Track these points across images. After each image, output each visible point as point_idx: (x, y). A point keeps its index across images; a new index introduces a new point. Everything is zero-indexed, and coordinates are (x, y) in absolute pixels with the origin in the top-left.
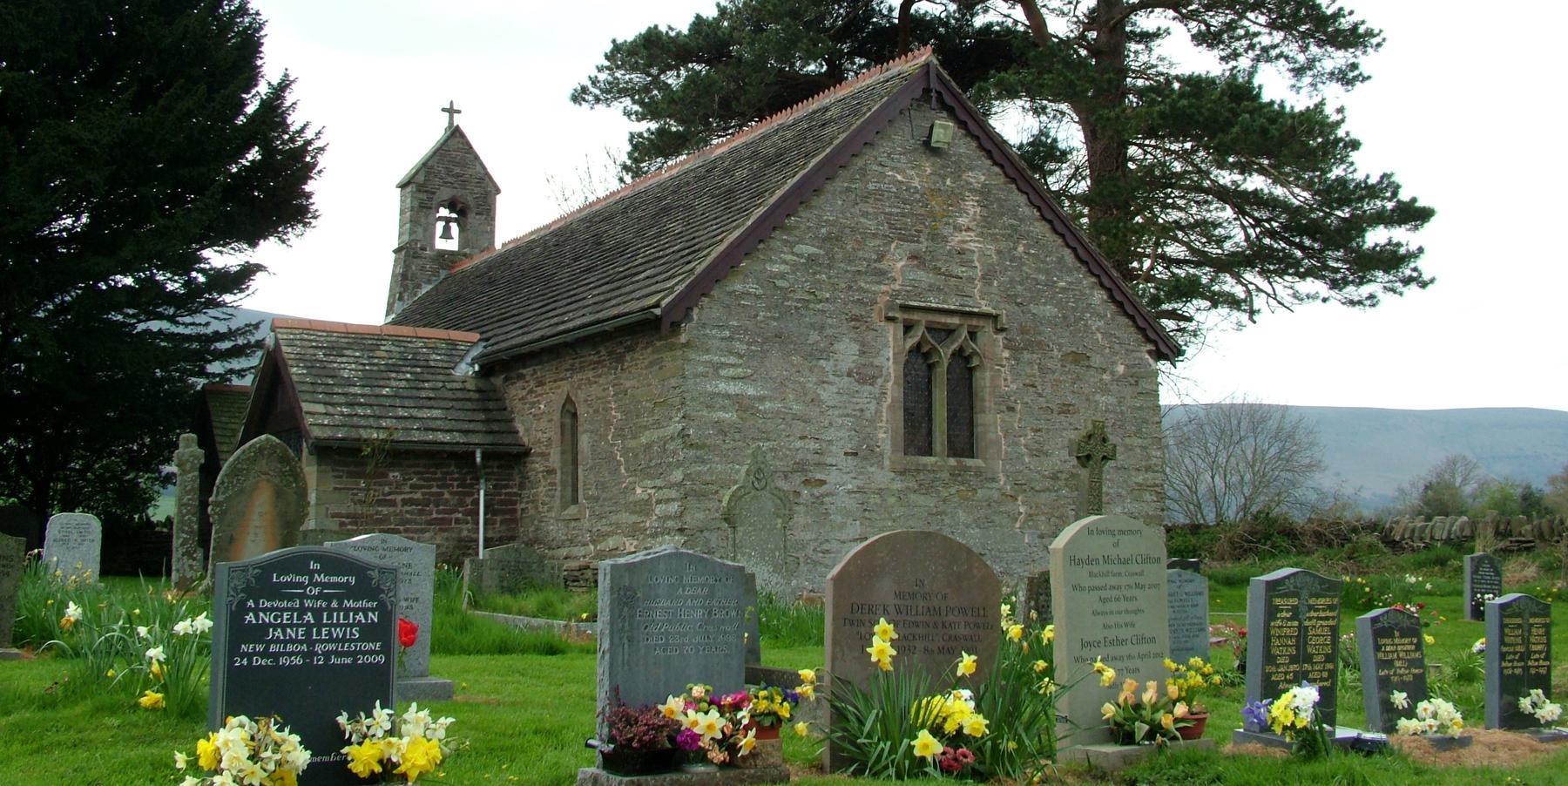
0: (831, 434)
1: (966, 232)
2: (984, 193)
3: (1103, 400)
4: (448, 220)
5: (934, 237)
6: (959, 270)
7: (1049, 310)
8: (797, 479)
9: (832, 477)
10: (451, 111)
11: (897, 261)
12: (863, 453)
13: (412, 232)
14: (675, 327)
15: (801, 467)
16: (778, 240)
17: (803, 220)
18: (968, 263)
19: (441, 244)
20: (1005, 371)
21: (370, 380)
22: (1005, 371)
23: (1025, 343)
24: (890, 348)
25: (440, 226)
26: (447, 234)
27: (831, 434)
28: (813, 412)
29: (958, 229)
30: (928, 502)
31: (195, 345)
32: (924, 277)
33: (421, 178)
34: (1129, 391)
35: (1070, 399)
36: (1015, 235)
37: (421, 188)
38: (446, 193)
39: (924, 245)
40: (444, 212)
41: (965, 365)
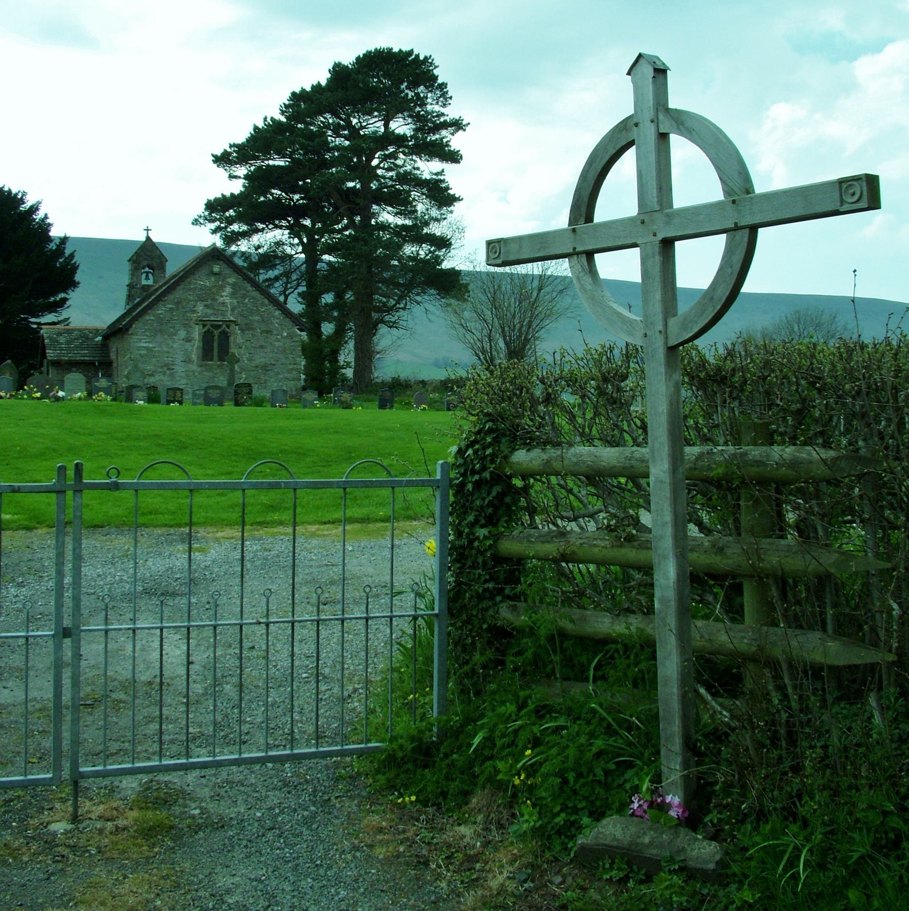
0: (176, 356)
1: (226, 296)
2: (234, 286)
3: (277, 344)
4: (147, 273)
5: (213, 299)
6: (223, 309)
7: (257, 318)
8: (165, 369)
9: (177, 368)
10: (147, 230)
11: (200, 308)
12: (187, 361)
13: (132, 279)
14: (127, 330)
15: (167, 365)
16: (160, 304)
17: (170, 297)
18: (227, 306)
19: (144, 282)
20: (239, 337)
21: (68, 343)
22: (239, 337)
23: (247, 328)
24: (197, 333)
25: (144, 276)
26: (147, 278)
27: (176, 356)
28: (171, 351)
29: (222, 296)
30: (210, 374)
31: (35, 326)
32: (209, 311)
33: (135, 258)
34: (288, 341)
35: (264, 344)
36: (244, 296)
37: (135, 262)
38: (145, 263)
39: (209, 302)
40: (147, 269)
41: (225, 336)
